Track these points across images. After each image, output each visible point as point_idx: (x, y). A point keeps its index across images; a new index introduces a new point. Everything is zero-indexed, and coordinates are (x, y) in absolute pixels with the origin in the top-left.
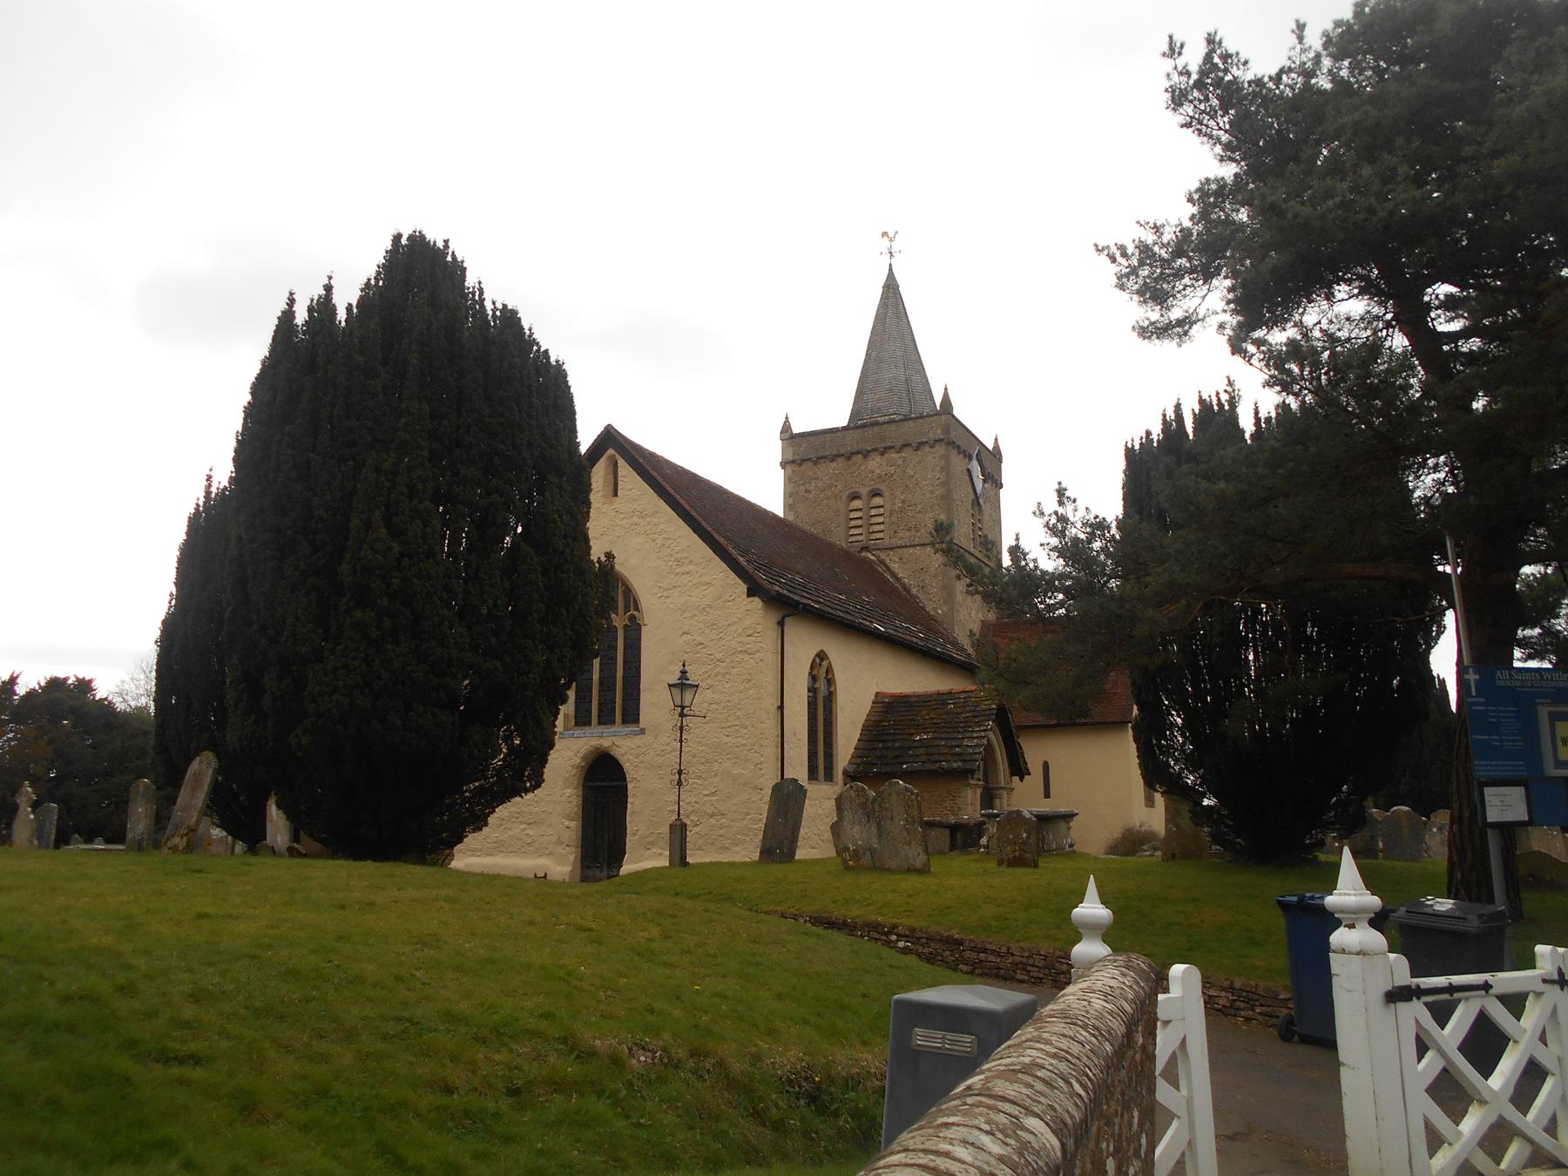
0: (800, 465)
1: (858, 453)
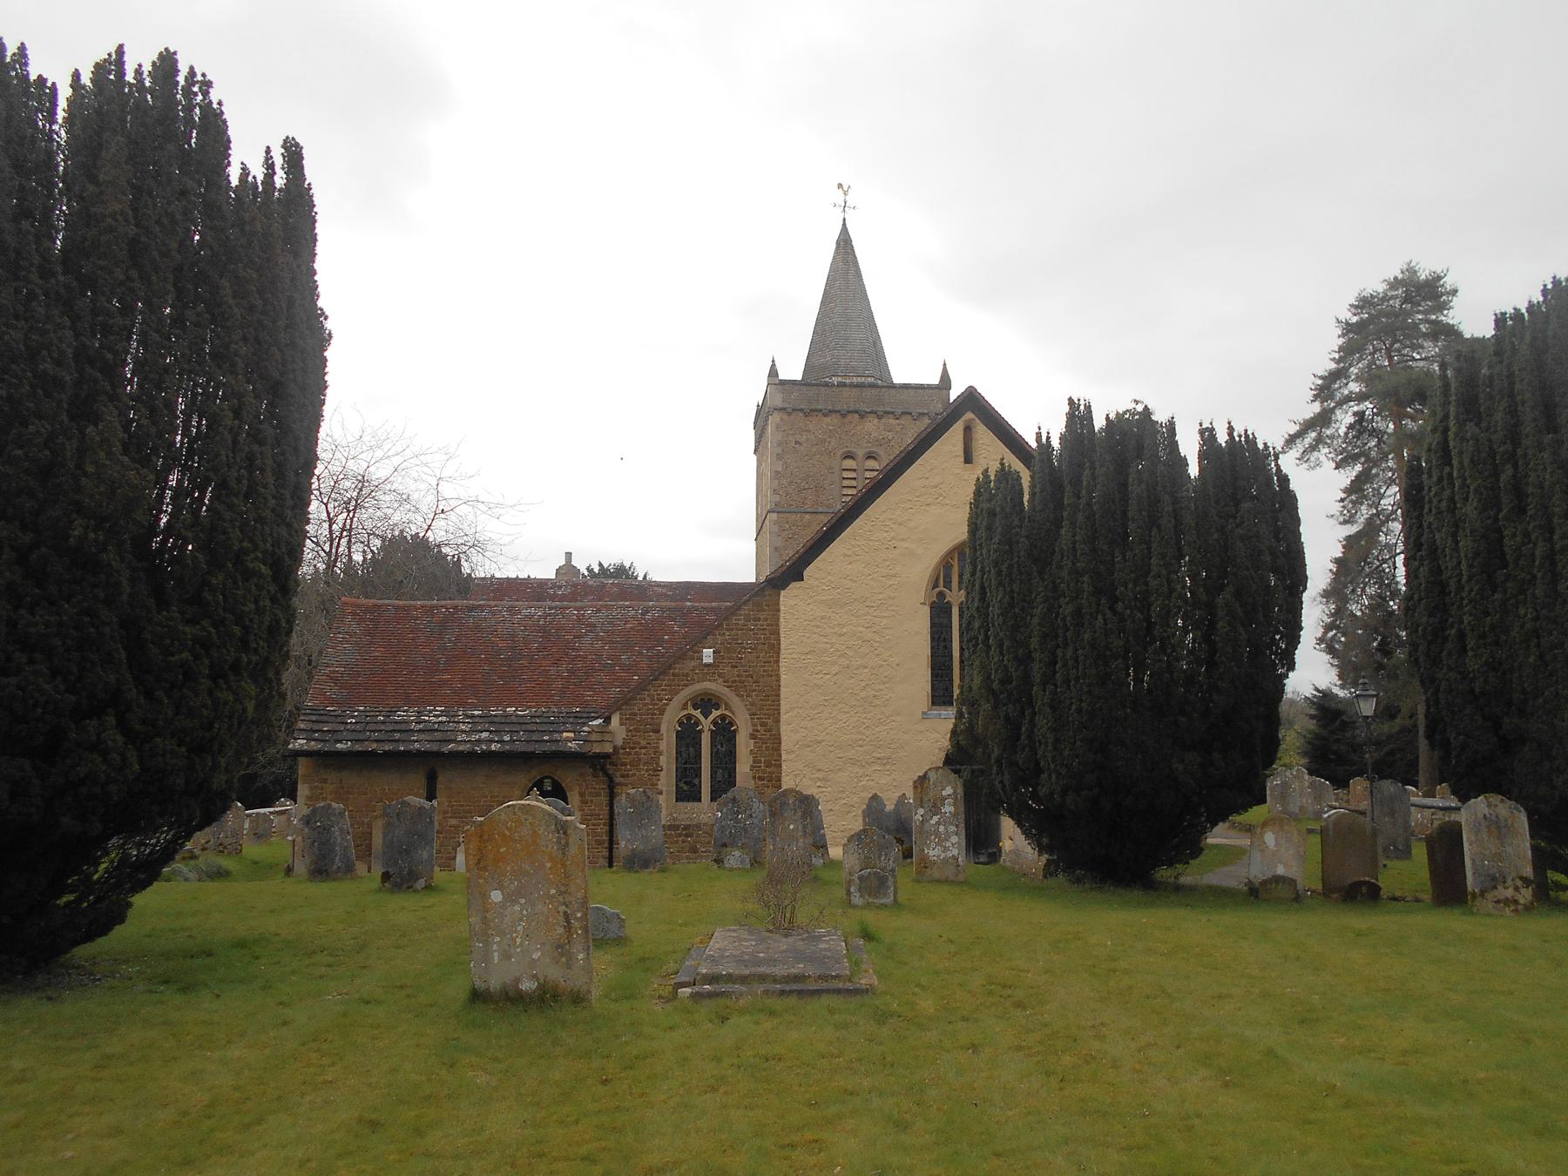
0: (789, 414)
1: (857, 412)
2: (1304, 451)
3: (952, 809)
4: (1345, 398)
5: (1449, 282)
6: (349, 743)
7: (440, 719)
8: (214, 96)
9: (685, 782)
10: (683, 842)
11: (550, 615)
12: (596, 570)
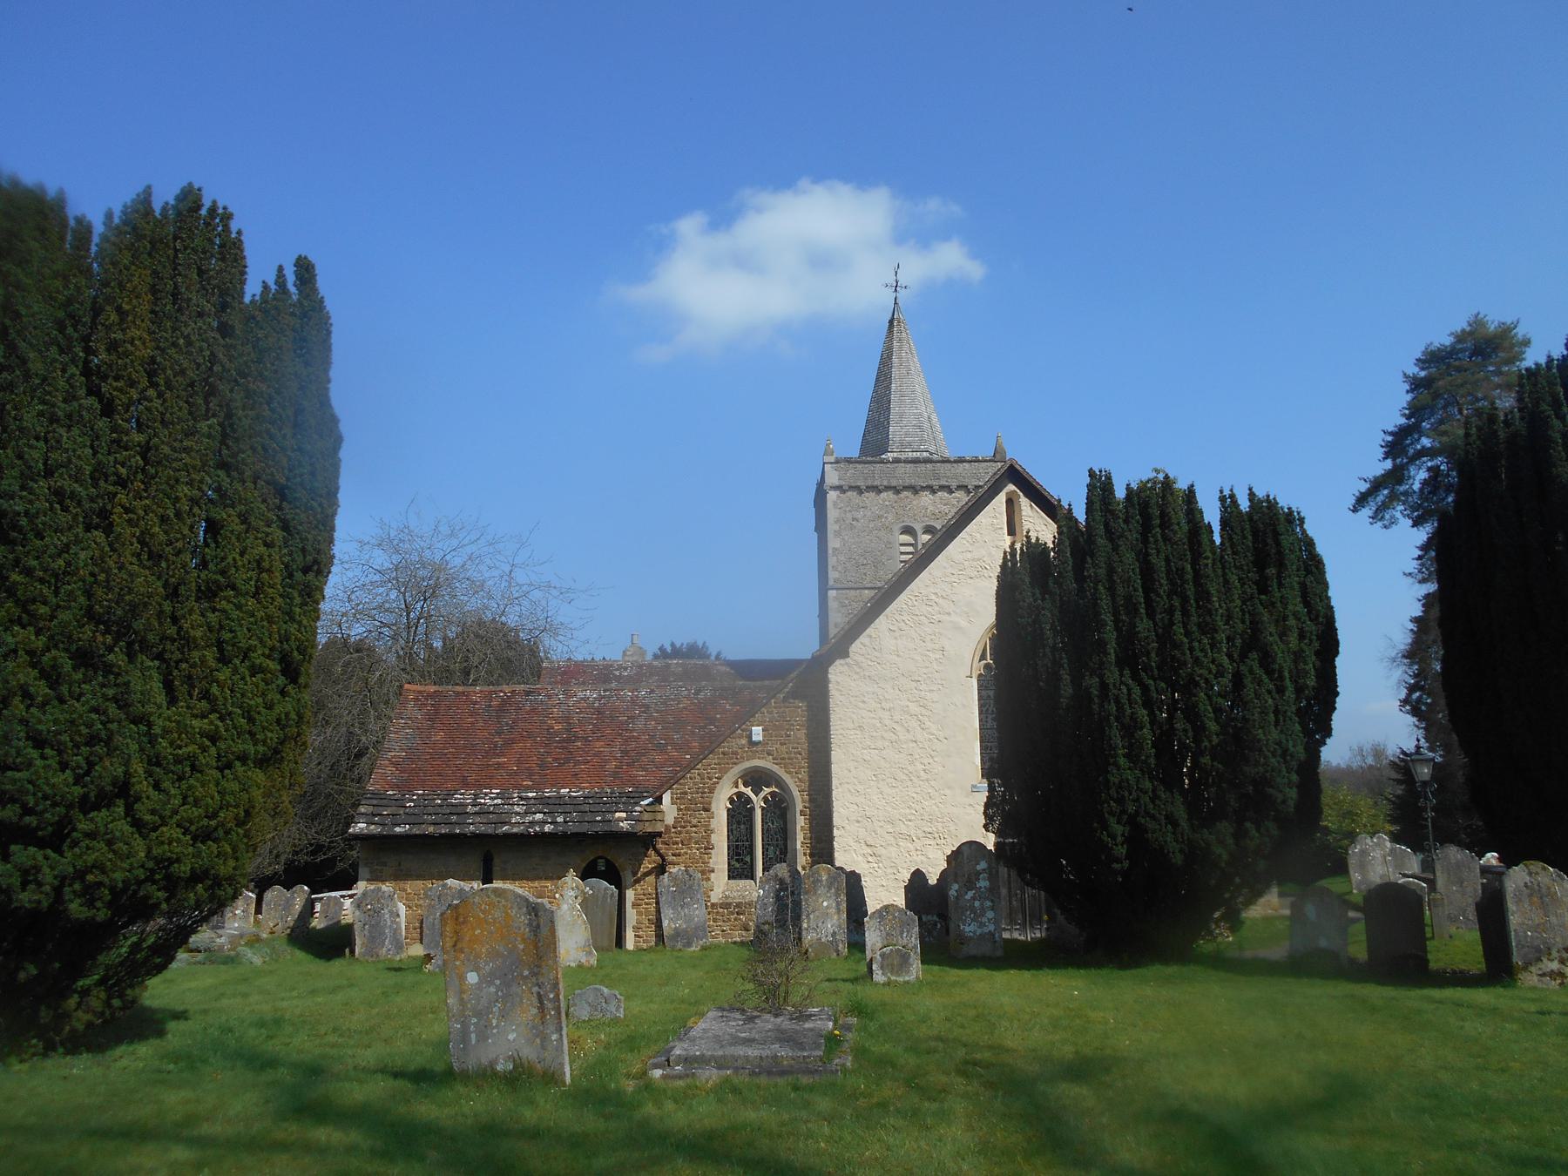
2: (1377, 509)
3: (987, 883)
4: (1417, 454)
5: (1520, 332)
6: (407, 826)
7: (496, 801)
8: (234, 226)
9: (737, 860)
10: (735, 919)
11: (604, 697)
12: (669, 650)
